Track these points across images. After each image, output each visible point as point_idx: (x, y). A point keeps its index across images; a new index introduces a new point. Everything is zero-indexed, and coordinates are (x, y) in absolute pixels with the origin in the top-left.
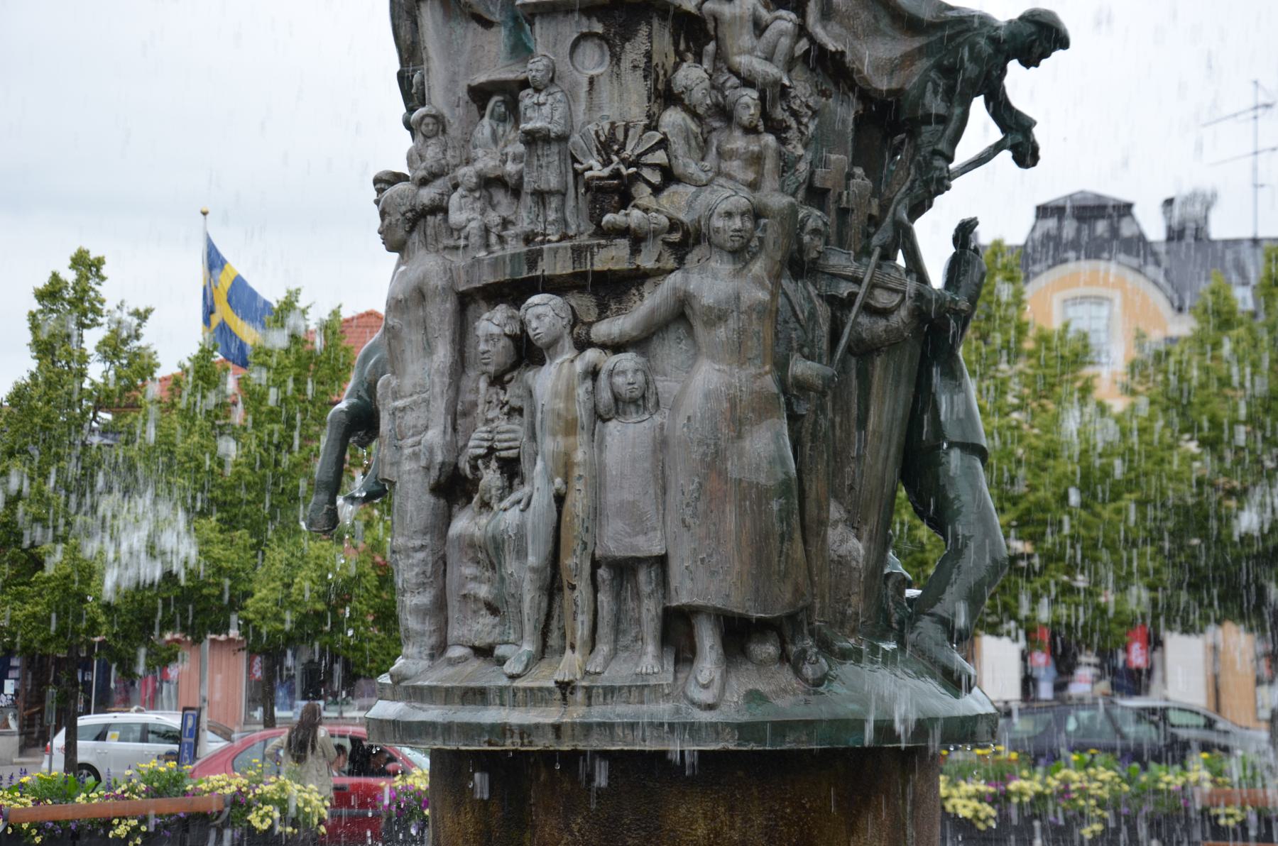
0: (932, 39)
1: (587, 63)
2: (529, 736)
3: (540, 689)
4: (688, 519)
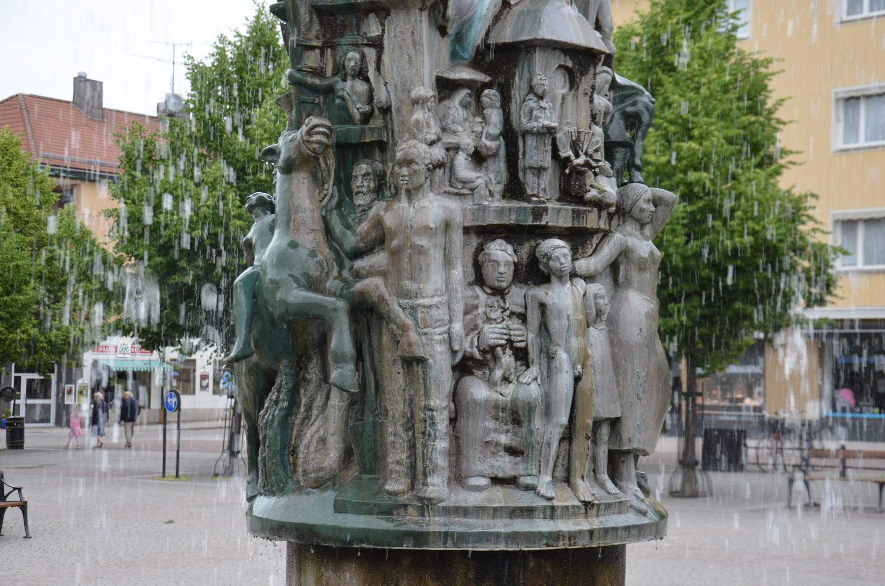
1: (557, 85)
4: (641, 395)
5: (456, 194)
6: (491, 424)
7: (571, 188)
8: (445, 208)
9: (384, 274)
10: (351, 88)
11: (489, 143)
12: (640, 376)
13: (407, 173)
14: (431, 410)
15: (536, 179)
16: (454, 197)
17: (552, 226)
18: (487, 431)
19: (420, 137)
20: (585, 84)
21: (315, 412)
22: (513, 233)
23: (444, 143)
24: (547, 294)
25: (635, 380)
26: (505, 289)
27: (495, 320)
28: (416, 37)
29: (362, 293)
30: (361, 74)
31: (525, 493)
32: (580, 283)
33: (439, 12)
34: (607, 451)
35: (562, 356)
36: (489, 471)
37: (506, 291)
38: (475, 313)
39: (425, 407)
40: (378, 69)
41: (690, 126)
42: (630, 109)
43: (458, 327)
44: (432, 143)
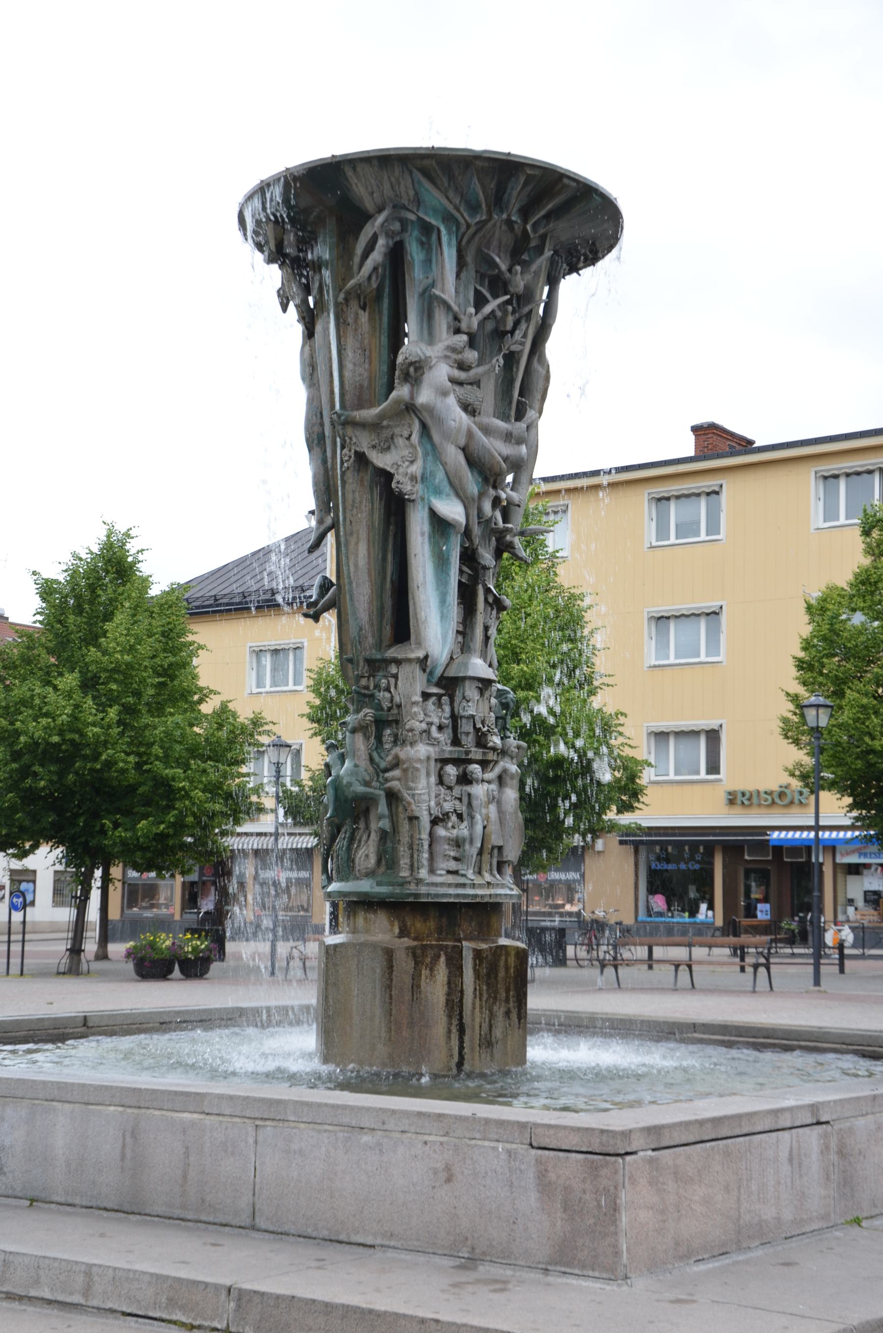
6: (447, 847)
7: (481, 741)
8: (428, 751)
9: (399, 779)
10: (383, 696)
11: (445, 721)
18: (445, 850)
20: (487, 694)
21: (363, 843)
22: (456, 762)
29: (390, 788)
30: (388, 689)
35: (478, 817)
36: (446, 868)
40: (396, 687)
41: (518, 650)
42: (504, 701)
43: (433, 803)
44: (421, 722)
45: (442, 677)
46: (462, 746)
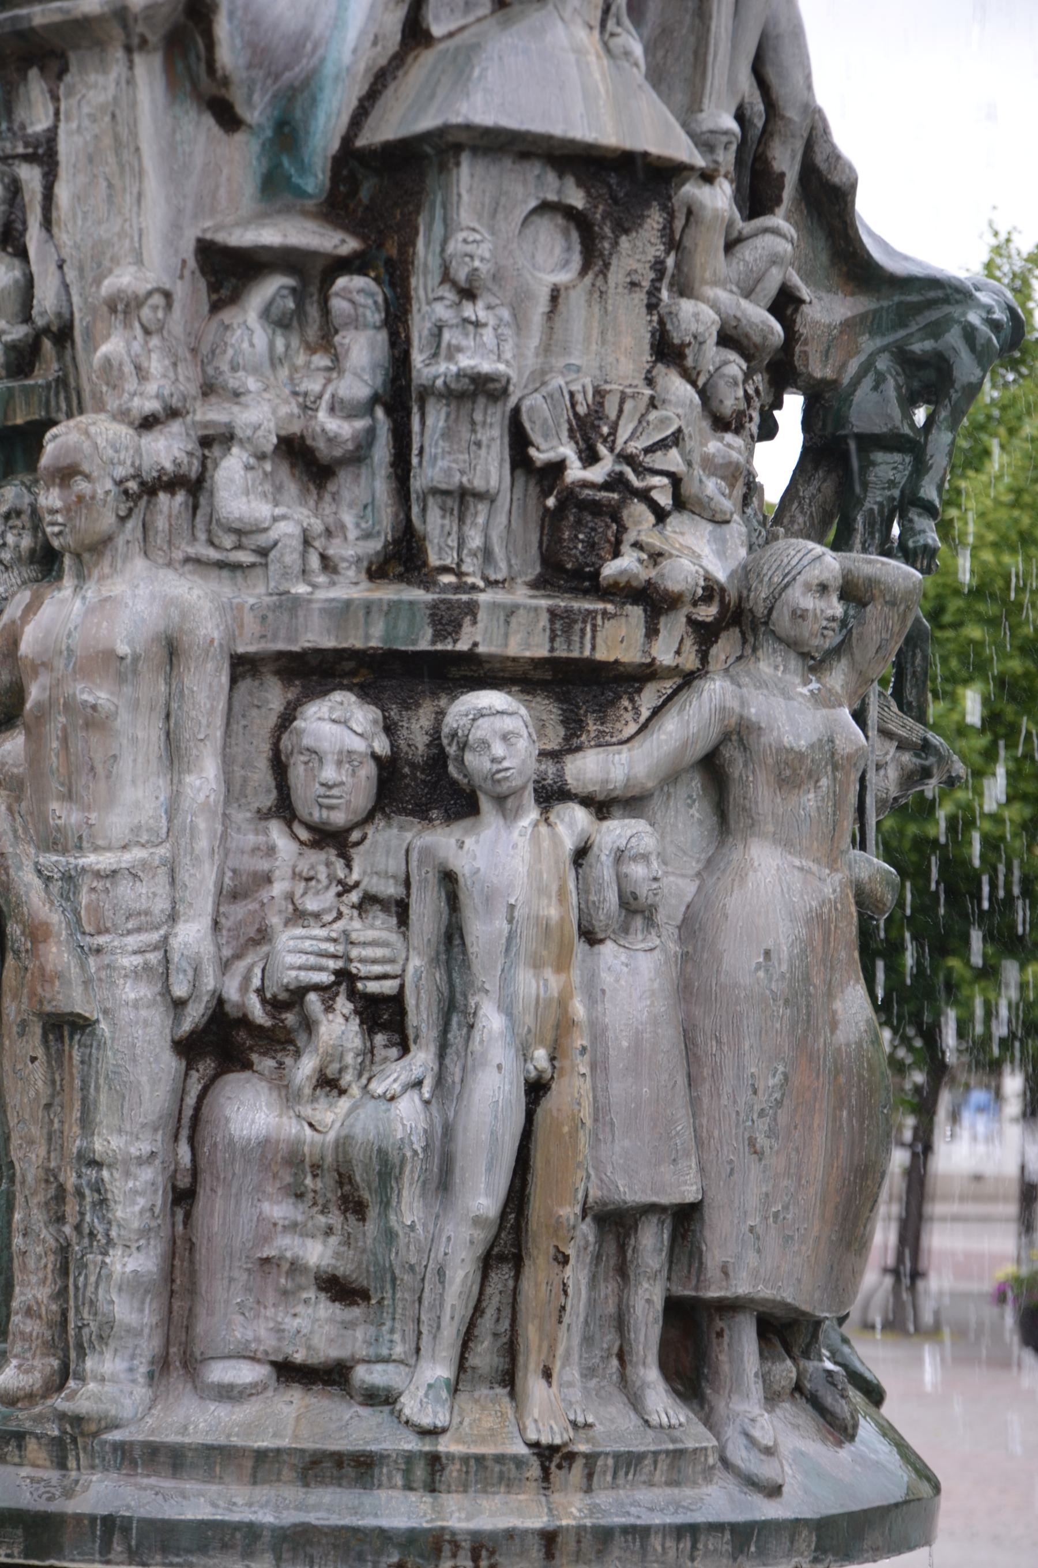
0: (885, 303)
1: (540, 258)
2: (492, 1553)
3: (500, 1459)
4: (761, 1141)
5: (221, 565)
6: (279, 1210)
7: (574, 536)
8: (169, 602)
12: (761, 1086)
13: (58, 504)
14: (96, 1164)
15: (451, 523)
16: (215, 573)
17: (491, 658)
18: (268, 1230)
19: (113, 404)
22: (393, 676)
23: (194, 423)
24: (461, 845)
25: (745, 1096)
26: (349, 830)
27: (317, 916)
28: (119, 129)
31: (364, 1411)
32: (575, 819)
33: (198, 58)
34: (659, 1304)
35: (491, 1020)
36: (268, 1342)
37: (355, 836)
38: (264, 895)
39: (80, 1156)
40: (47, 223)
42: (920, 347)
43: (192, 934)
44: (148, 423)
45: (350, 159)
46: (427, 582)
